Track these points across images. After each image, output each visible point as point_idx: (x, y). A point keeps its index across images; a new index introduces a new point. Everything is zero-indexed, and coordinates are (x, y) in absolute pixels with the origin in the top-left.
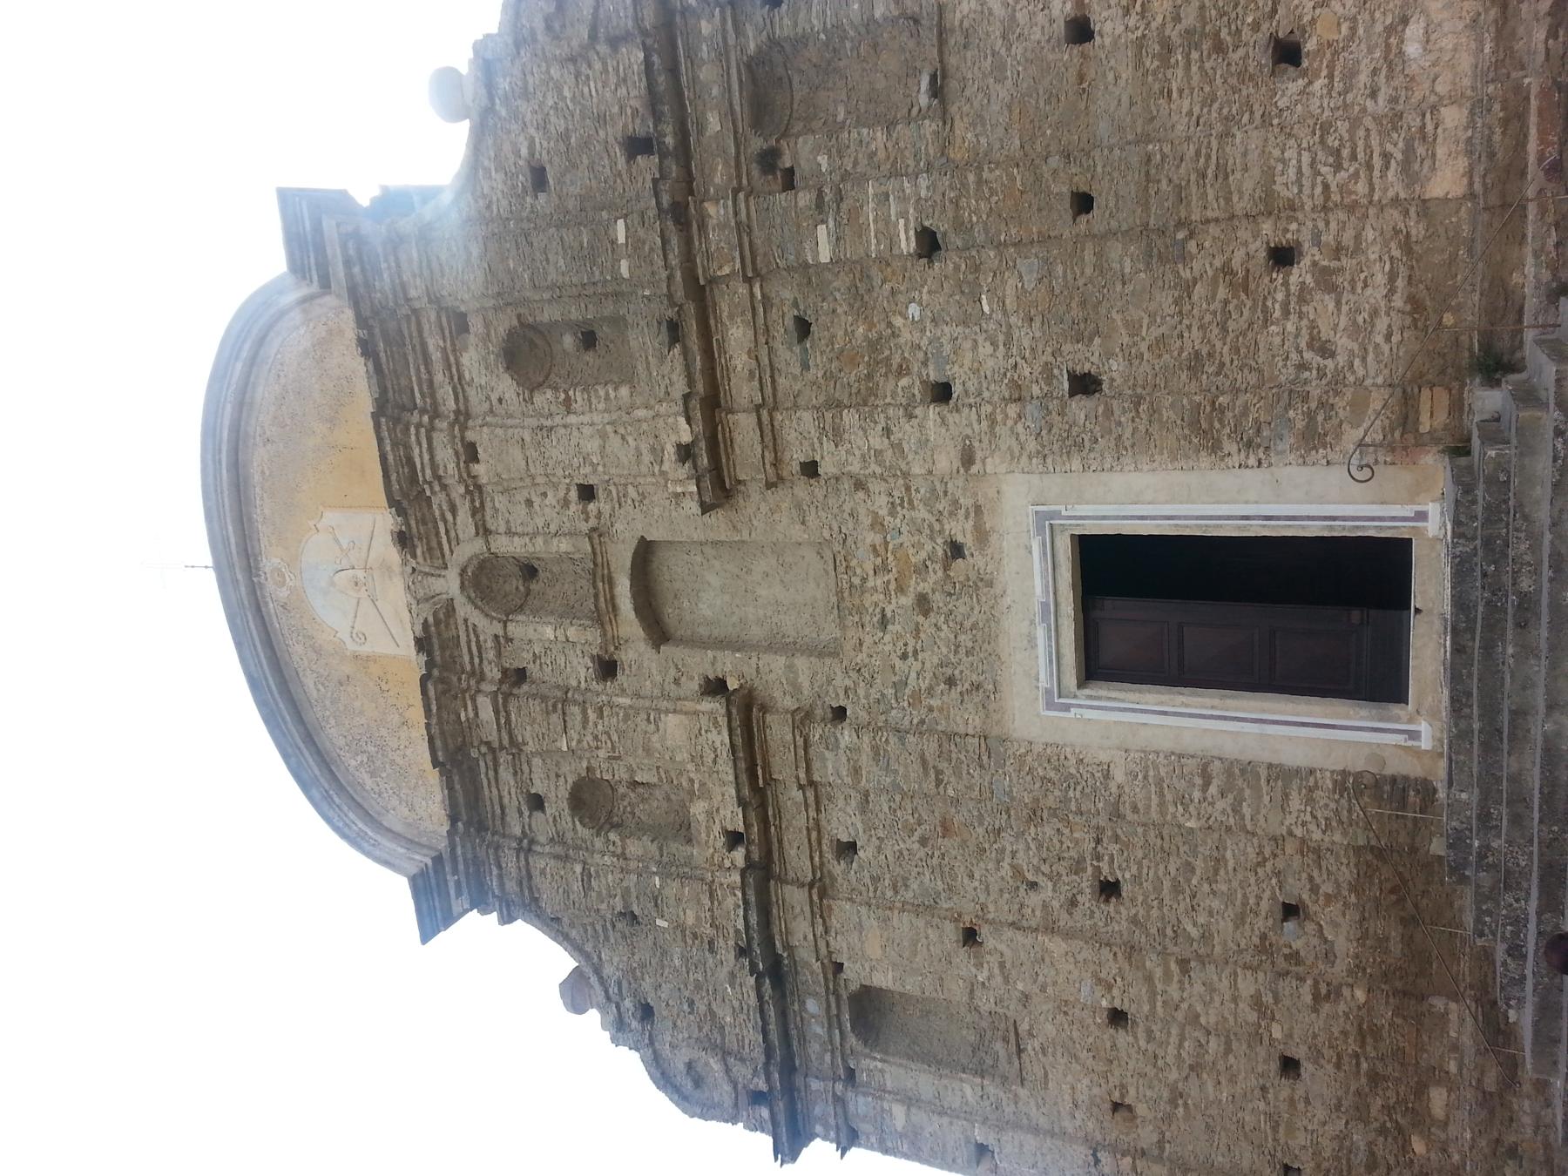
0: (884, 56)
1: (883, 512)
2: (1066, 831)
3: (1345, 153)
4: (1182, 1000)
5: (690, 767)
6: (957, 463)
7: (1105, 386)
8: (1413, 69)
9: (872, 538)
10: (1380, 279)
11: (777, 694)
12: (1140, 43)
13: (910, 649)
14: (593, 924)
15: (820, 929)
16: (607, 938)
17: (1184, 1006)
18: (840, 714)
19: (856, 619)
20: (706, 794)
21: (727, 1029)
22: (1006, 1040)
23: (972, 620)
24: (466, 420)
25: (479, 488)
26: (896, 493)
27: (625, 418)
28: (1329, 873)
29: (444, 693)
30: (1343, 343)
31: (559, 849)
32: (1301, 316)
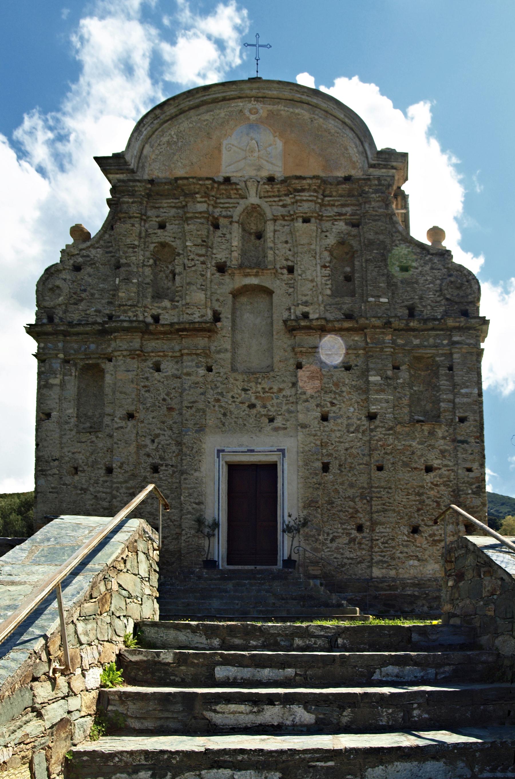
0: (431, 405)
1: (284, 393)
2: (175, 455)
3: (386, 545)
4: (120, 493)
5: (184, 302)
6: (300, 421)
7: (325, 474)
8: (407, 563)
9: (275, 389)
10: (352, 555)
11: (215, 344)
12: (423, 487)
13: (235, 400)
14: (112, 246)
15: (125, 353)
16: (107, 253)
17: (118, 494)
18: (210, 369)
19: (246, 379)
20: (174, 307)
21: (76, 306)
22: (91, 427)
23: (247, 424)
24: (319, 220)
25: (292, 220)
26: (291, 398)
27: (319, 291)
28: (171, 542)
29: (207, 188)
30: (334, 545)
31: (143, 234)
32: (343, 533)
